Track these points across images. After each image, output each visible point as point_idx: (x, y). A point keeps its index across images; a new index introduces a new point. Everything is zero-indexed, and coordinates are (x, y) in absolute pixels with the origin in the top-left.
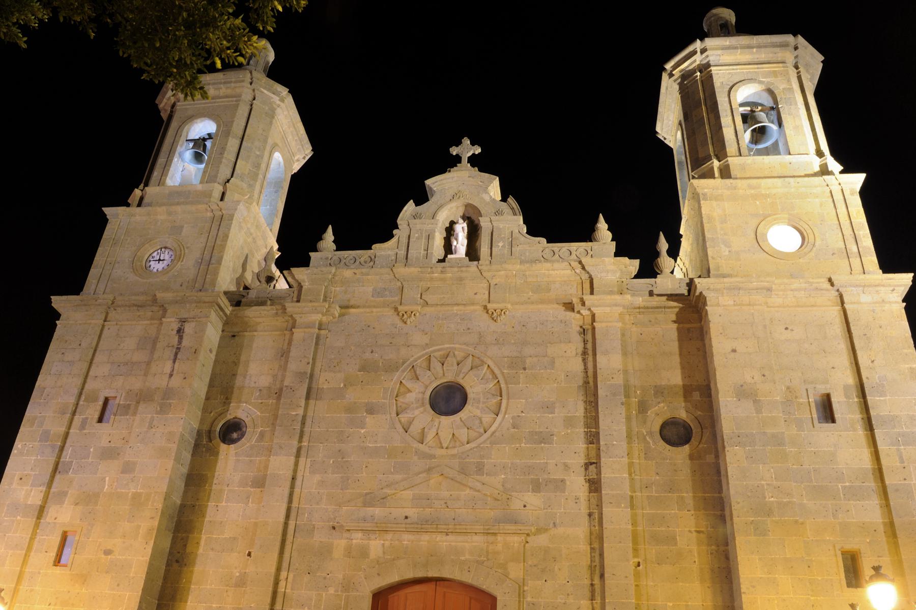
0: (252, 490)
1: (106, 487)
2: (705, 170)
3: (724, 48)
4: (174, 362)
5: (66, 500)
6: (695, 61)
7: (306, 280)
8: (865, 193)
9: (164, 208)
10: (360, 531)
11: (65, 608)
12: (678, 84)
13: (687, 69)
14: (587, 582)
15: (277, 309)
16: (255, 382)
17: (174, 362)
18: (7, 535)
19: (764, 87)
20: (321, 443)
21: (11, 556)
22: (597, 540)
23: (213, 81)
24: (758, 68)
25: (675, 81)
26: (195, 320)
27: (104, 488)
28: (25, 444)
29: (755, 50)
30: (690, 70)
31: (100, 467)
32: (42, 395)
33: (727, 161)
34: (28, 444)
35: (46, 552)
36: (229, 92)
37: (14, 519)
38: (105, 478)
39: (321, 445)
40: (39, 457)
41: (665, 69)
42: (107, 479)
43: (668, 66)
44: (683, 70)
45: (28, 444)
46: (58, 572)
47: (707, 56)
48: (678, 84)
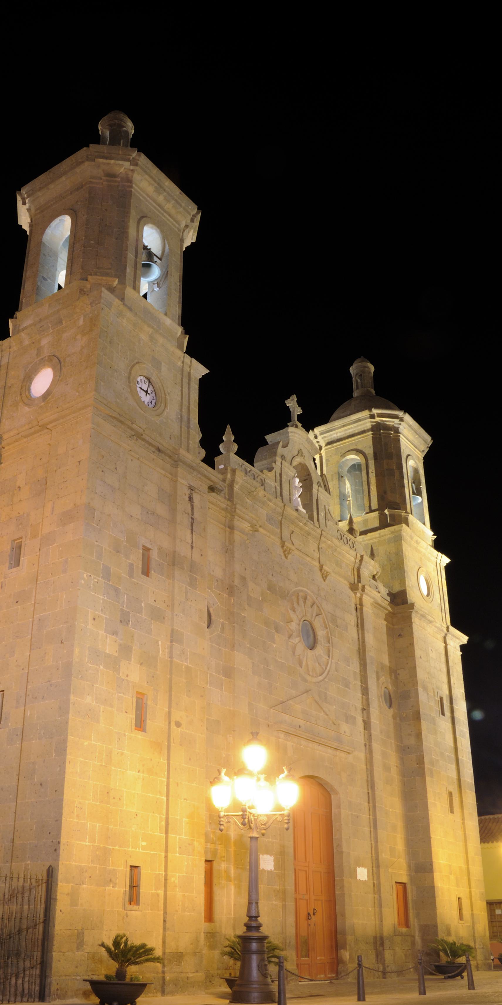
0: (224, 678)
1: (161, 652)
2: (396, 513)
3: (410, 426)
4: (192, 533)
5: (132, 656)
6: (393, 422)
7: (239, 484)
8: (448, 568)
9: (150, 330)
10: (284, 733)
11: (151, 777)
12: (372, 425)
13: (385, 423)
14: (366, 791)
15: (228, 505)
16: (213, 571)
17: (192, 533)
18: (95, 685)
19: (415, 466)
20: (256, 648)
21: (103, 712)
22: (370, 761)
23: (169, 190)
24: (414, 449)
25: (371, 422)
26: (200, 493)
27: (159, 652)
28: (90, 576)
29: (417, 436)
30: (386, 424)
31: (152, 627)
32: (94, 517)
33: (408, 516)
34: (93, 576)
35: (126, 712)
36: (173, 212)
37: (98, 667)
38: (157, 642)
39: (256, 650)
40: (106, 598)
41: (370, 410)
42: (160, 643)
43: (375, 411)
44: (382, 421)
45: (93, 576)
46: (140, 737)
47: (400, 424)
48: (372, 425)
